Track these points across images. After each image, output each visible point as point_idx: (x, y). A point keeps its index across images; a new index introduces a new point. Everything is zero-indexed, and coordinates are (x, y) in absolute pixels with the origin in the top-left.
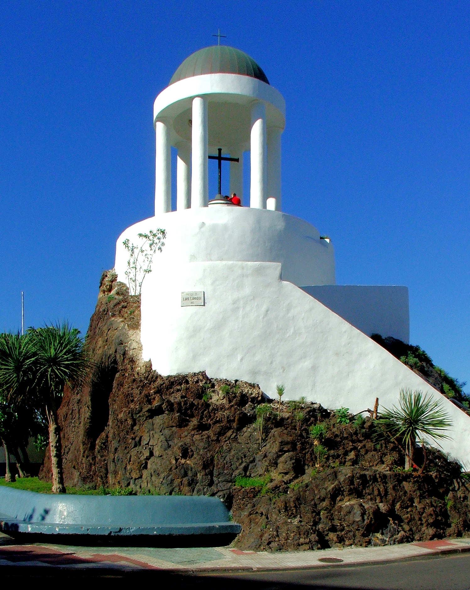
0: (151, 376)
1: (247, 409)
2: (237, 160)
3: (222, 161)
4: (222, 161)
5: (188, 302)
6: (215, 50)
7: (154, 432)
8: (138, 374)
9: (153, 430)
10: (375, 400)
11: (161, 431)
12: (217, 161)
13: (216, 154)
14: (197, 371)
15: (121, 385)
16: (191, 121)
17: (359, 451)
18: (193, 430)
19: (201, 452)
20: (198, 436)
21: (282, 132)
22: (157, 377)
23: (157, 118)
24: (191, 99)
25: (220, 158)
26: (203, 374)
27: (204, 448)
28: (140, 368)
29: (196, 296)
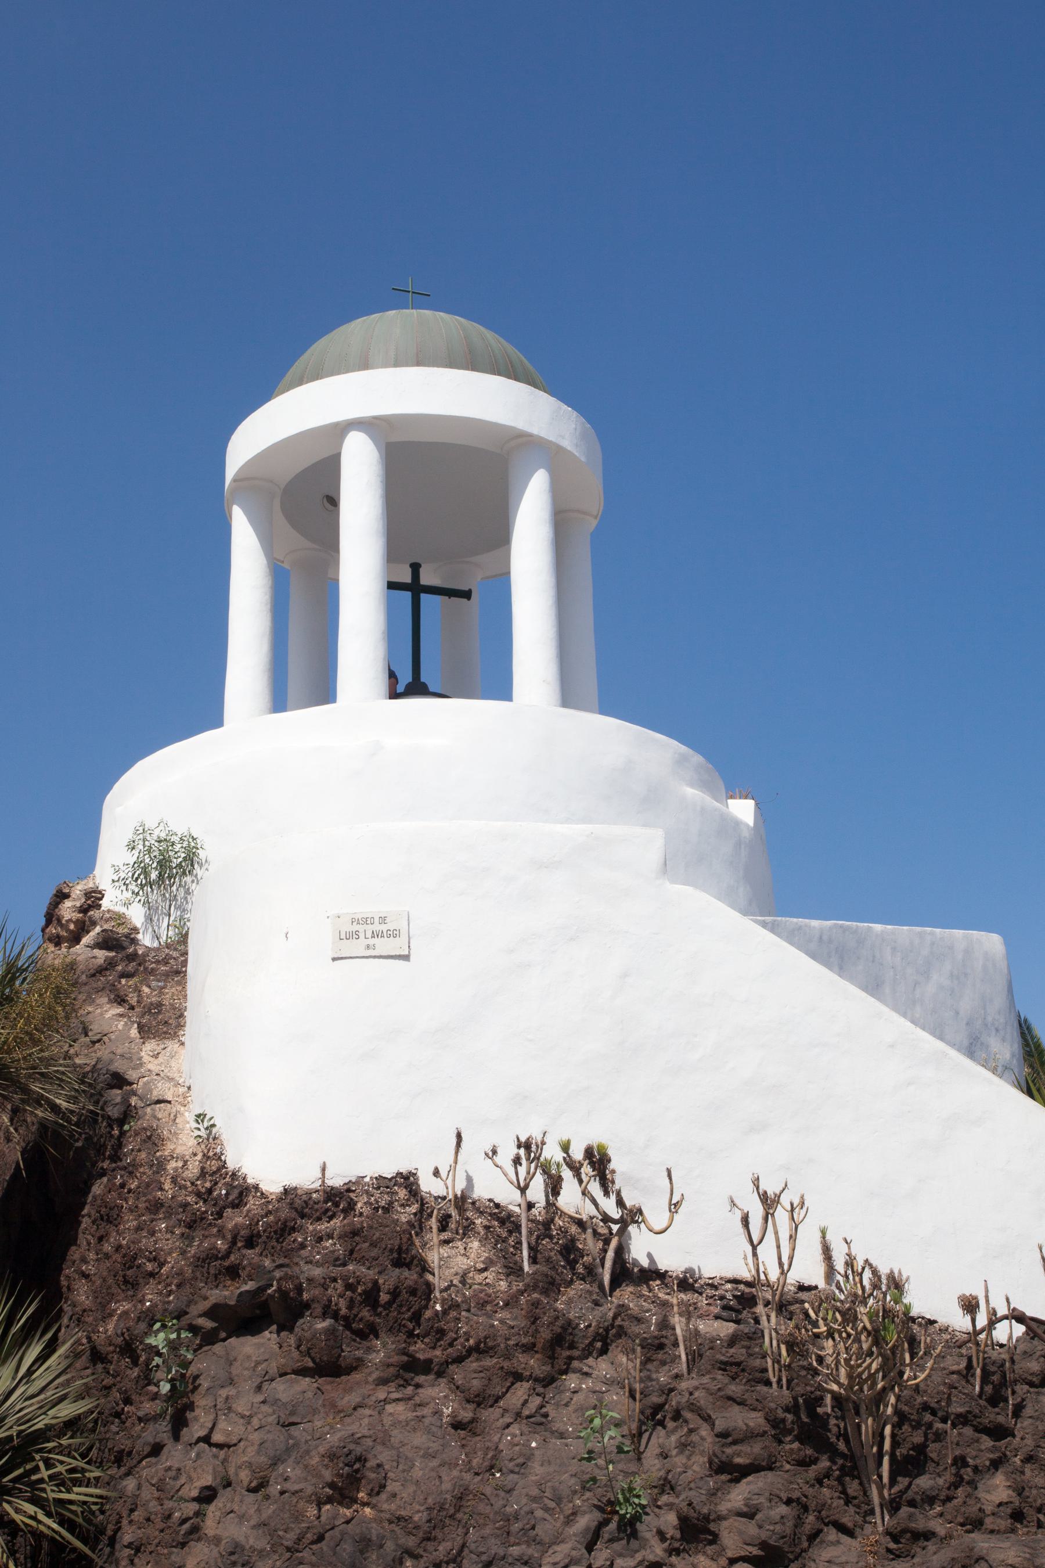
0: (222, 1189)
1: (574, 1303)
2: (467, 595)
3: (423, 596)
4: (423, 596)
5: (357, 947)
6: (395, 323)
7: (232, 1392)
8: (174, 1180)
9: (231, 1382)
10: (819, 1234)
11: (259, 1388)
12: (409, 594)
13: (406, 578)
14: (388, 1171)
15: (109, 1217)
16: (333, 501)
17: (574, 1274)
18: (383, 1382)
19: (417, 1473)
20: (400, 1407)
21: (594, 523)
22: (242, 1191)
23: (235, 480)
24: (340, 430)
25: (415, 588)
26: (408, 1181)
27: (429, 1455)
28: (183, 1142)
29: (384, 928)
